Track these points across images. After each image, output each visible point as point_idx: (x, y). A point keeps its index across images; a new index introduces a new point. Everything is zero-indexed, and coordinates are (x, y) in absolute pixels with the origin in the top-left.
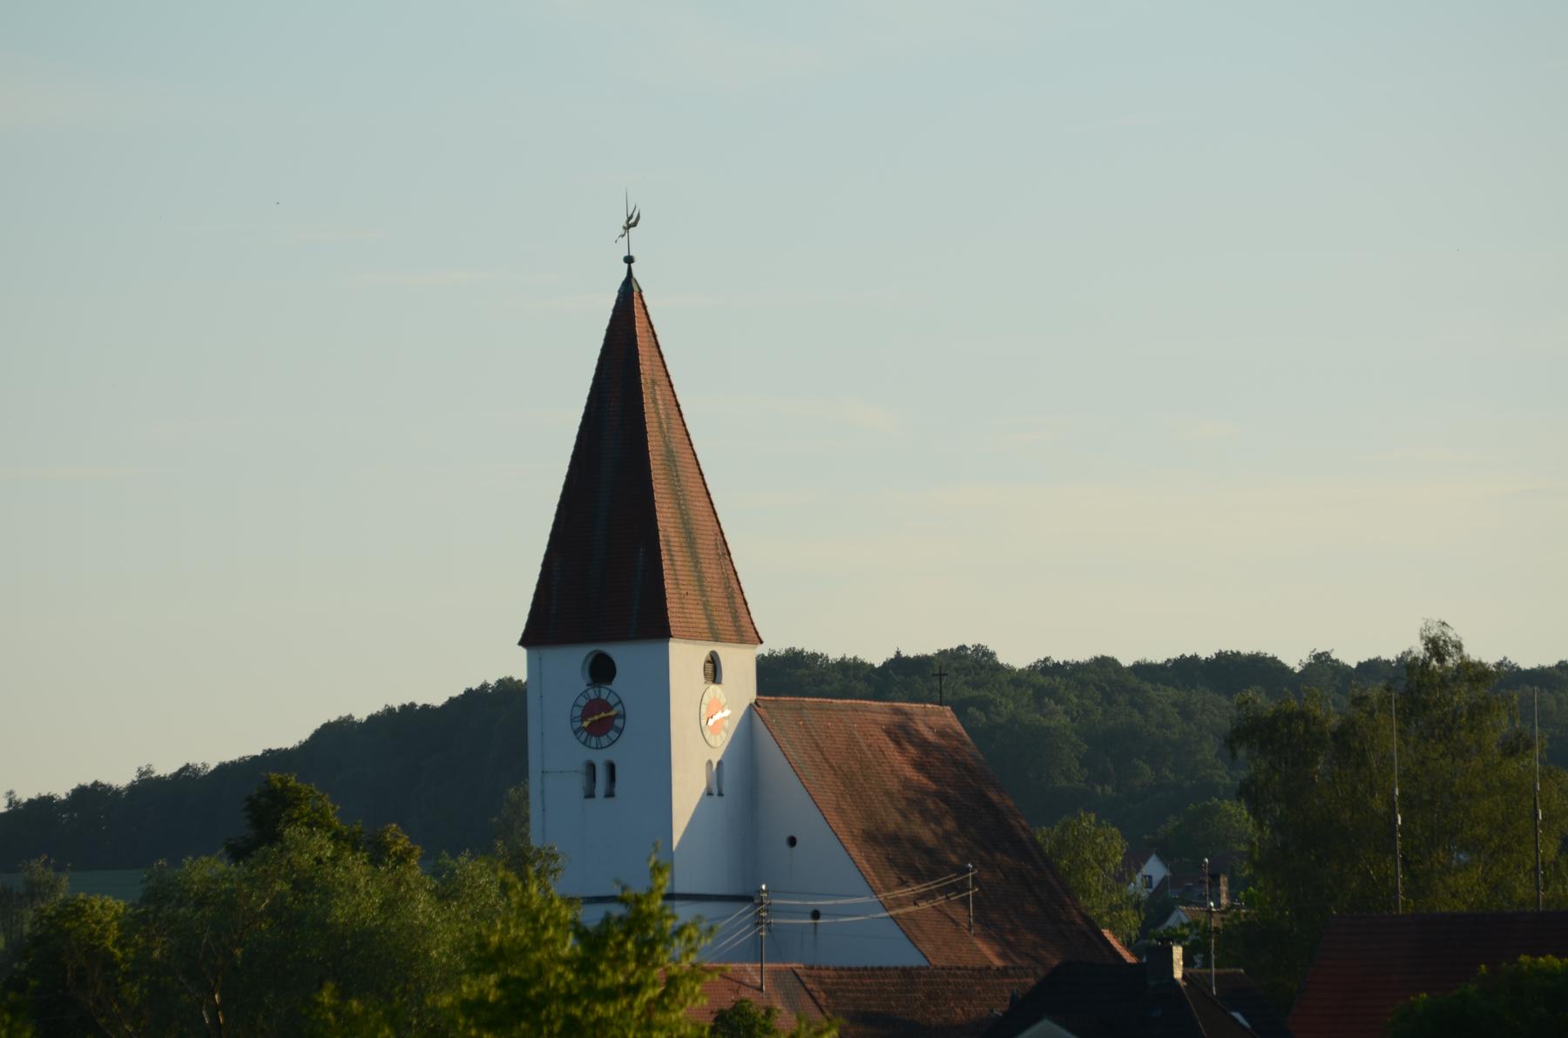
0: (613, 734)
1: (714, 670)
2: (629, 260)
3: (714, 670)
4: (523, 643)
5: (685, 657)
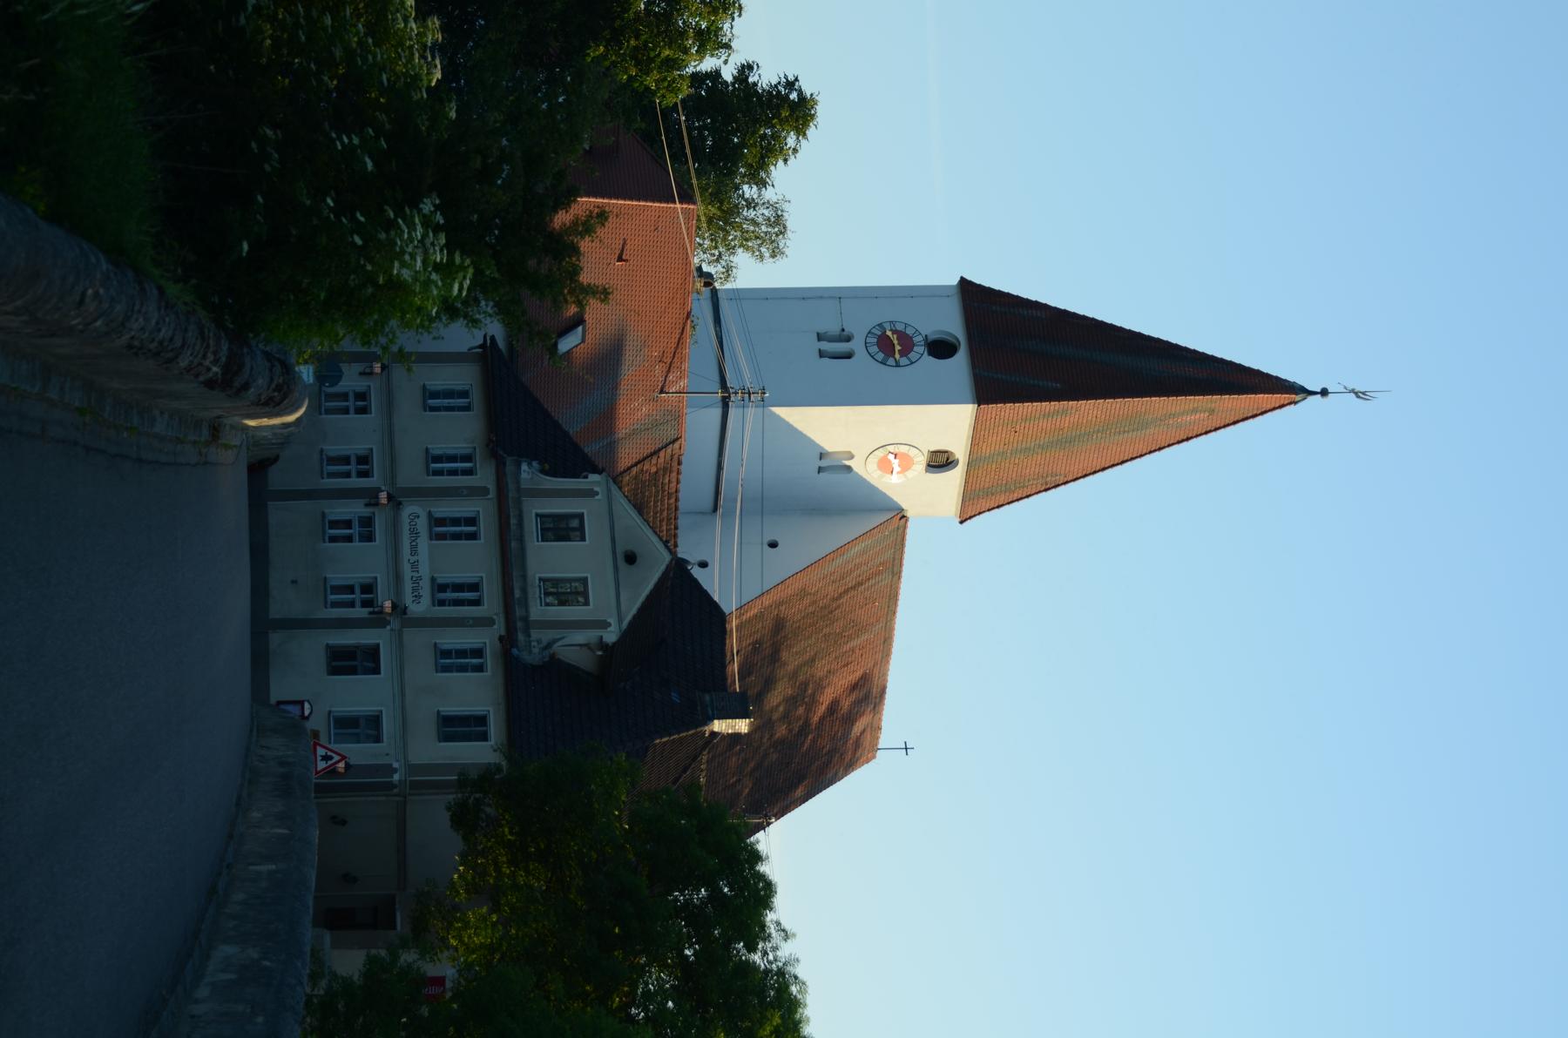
0: (880, 356)
1: (940, 462)
2: (1324, 392)
3: (940, 462)
4: (963, 281)
5: (952, 423)
